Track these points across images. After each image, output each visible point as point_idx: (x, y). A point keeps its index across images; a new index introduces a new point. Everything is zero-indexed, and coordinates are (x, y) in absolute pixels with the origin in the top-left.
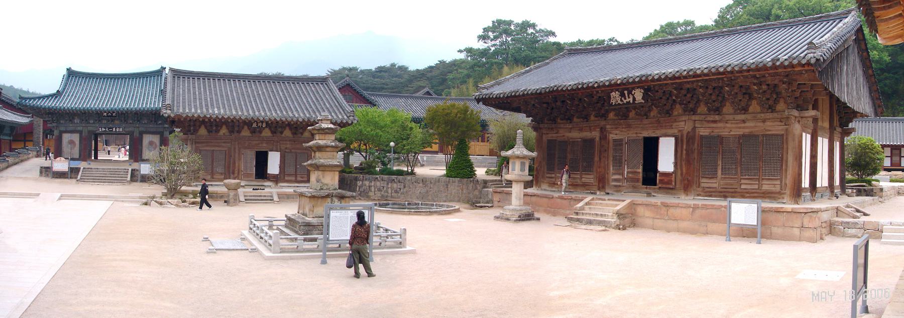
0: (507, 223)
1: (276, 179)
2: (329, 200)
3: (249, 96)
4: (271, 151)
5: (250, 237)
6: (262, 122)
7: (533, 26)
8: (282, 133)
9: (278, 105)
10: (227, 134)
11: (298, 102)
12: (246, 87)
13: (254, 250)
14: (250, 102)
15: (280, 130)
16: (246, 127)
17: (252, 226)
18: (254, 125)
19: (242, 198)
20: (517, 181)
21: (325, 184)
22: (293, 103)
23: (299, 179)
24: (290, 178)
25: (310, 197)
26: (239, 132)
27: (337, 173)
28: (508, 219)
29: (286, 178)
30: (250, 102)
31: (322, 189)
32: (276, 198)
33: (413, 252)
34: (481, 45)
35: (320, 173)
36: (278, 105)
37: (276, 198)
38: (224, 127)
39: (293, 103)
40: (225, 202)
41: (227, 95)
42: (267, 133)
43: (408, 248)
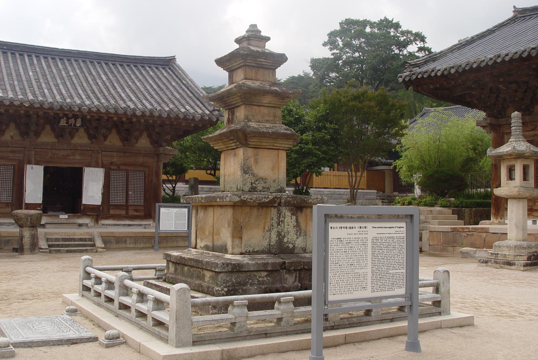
0: (506, 272)
1: (97, 213)
2: (274, 211)
3: (54, 78)
4: (89, 166)
5: (87, 305)
6: (75, 117)
7: (397, 26)
8: (105, 137)
9: (101, 92)
10: (18, 138)
11: (131, 89)
12: (49, 66)
13: (115, 341)
14: (57, 85)
15: (103, 131)
16: (48, 128)
17: (89, 283)
18: (63, 122)
19: (43, 244)
20: (514, 198)
21: (259, 179)
22: (125, 91)
23: (131, 213)
24: (117, 212)
25: (234, 206)
26: (37, 134)
27: (283, 154)
28: (509, 264)
29: (112, 212)
30: (57, 85)
31: (253, 189)
32: (99, 243)
33: (465, 324)
34: (326, 53)
35: (250, 152)
36: (101, 92)
37: (99, 243)
38: (12, 125)
39: (125, 91)
40: (15, 250)
41: (19, 75)
42: (81, 139)
43: (456, 314)
